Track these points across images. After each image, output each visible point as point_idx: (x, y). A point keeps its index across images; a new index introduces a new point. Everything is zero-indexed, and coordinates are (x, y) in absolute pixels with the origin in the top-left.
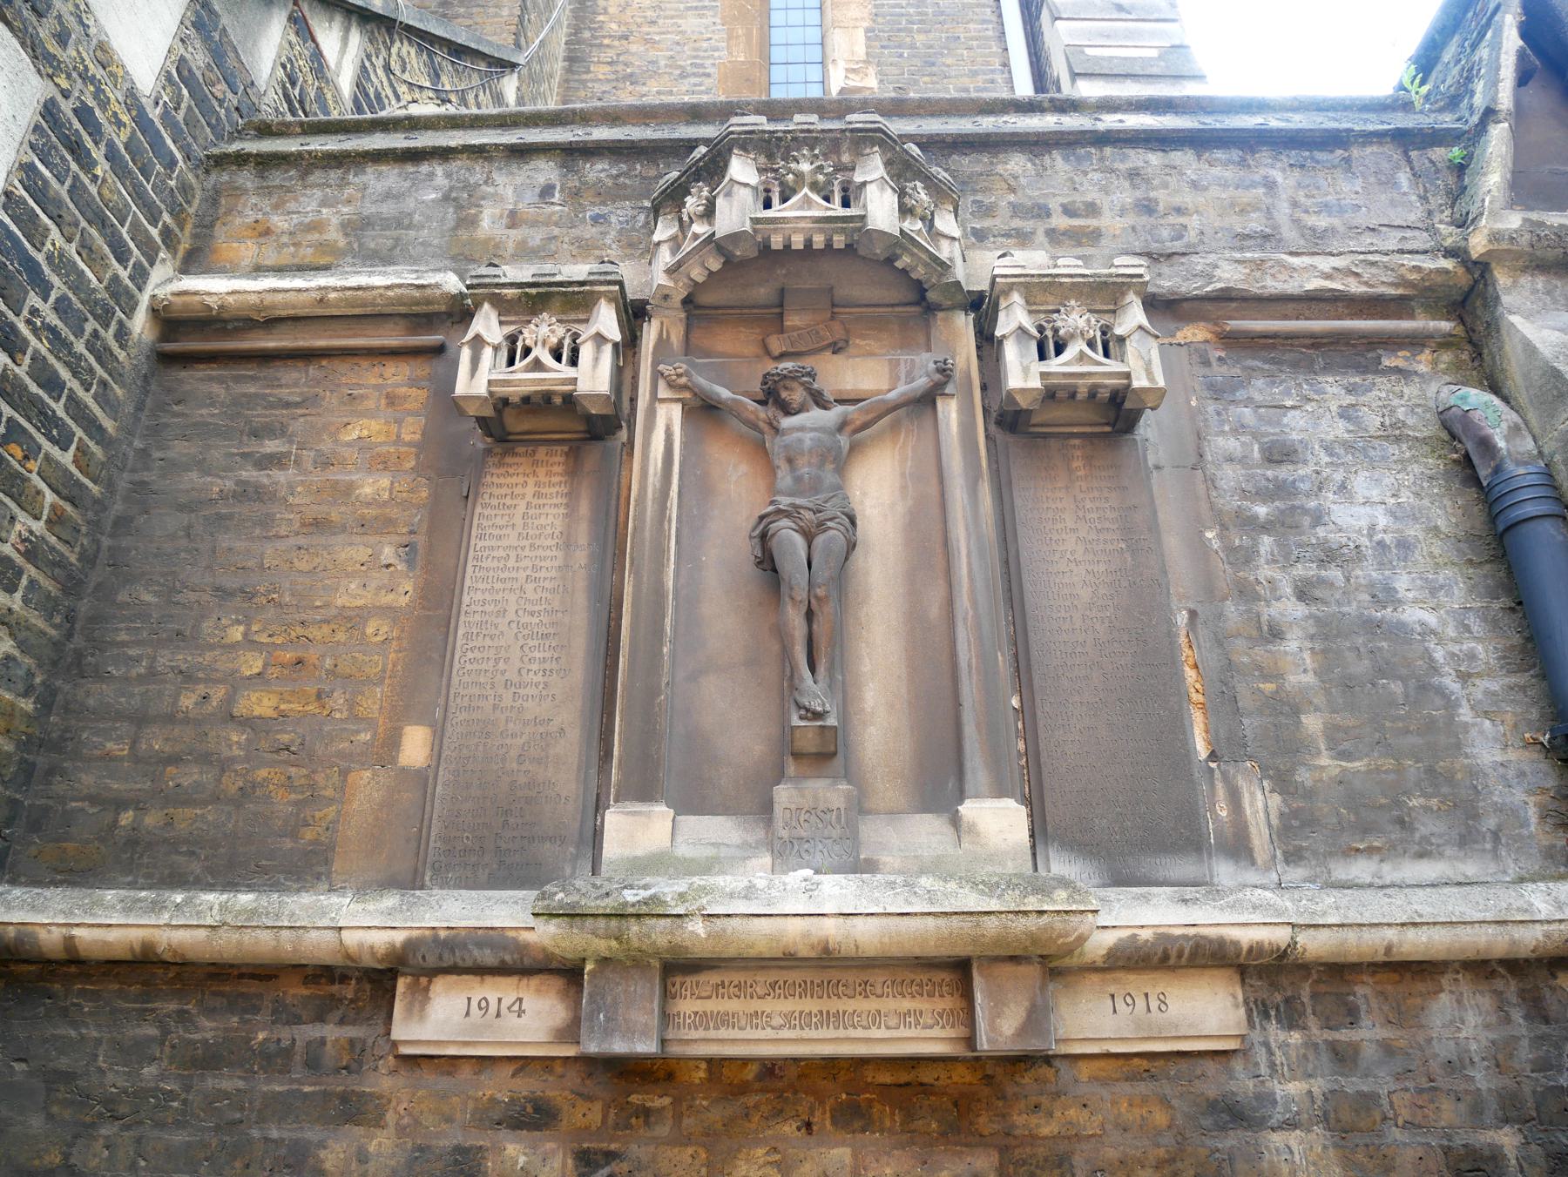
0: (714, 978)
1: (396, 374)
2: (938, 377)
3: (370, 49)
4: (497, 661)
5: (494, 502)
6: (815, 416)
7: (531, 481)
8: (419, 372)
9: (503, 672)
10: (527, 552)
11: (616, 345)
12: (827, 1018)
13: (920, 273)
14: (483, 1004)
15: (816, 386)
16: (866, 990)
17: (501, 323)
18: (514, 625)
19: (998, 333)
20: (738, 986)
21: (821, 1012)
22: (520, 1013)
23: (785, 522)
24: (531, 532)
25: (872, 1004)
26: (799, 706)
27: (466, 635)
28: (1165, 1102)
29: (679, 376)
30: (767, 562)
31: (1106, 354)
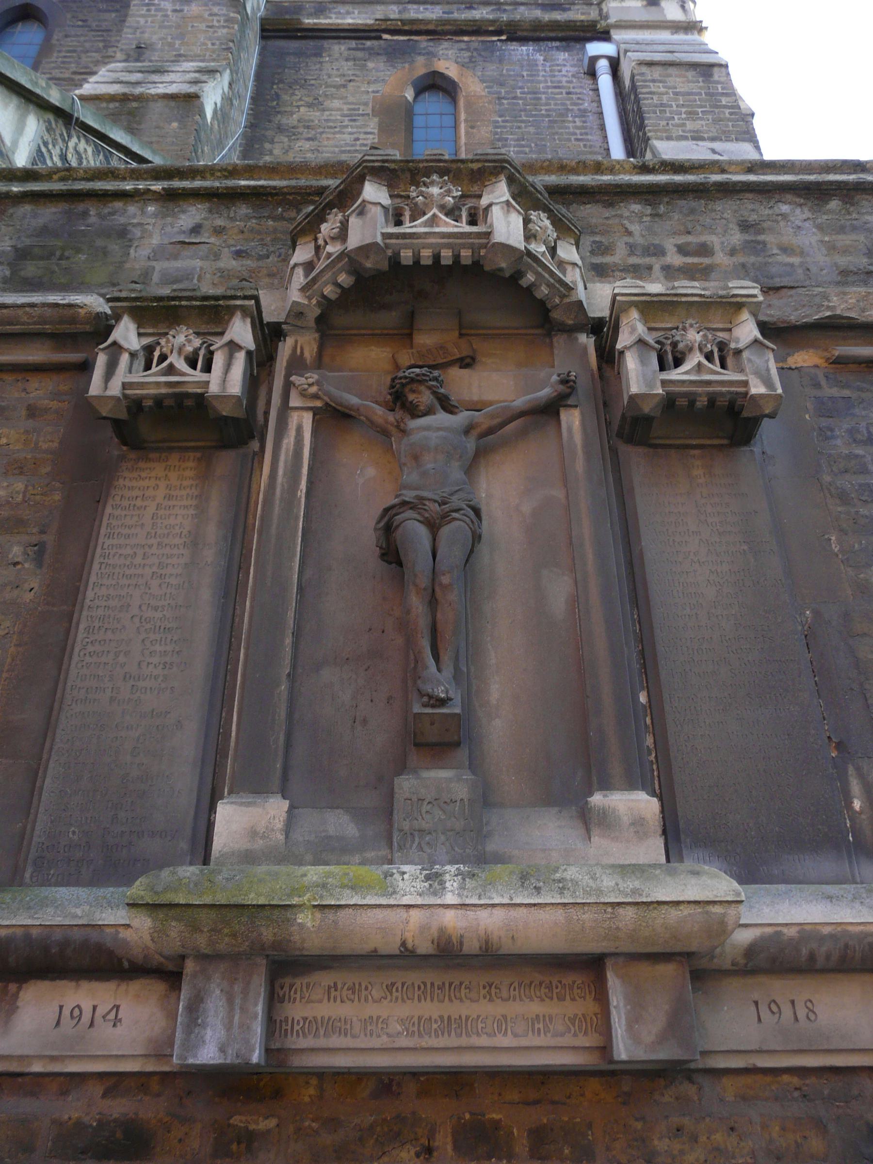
0: (325, 979)
1: (39, 390)
2: (561, 388)
3: (47, 137)
4: (117, 655)
5: (125, 503)
6: (441, 418)
7: (162, 484)
8: (63, 388)
9: (123, 666)
10: (154, 550)
11: (249, 353)
12: (448, 1024)
13: (543, 291)
14: (76, 1012)
15: (442, 391)
16: (490, 991)
17: (140, 335)
18: (137, 620)
19: (619, 346)
20: (352, 989)
21: (441, 1017)
22: (116, 1022)
23: (410, 514)
24: (159, 532)
25: (496, 1009)
26: (421, 694)
27: (88, 629)
28: (820, 1126)
29: (310, 385)
30: (392, 554)
31: (723, 366)
